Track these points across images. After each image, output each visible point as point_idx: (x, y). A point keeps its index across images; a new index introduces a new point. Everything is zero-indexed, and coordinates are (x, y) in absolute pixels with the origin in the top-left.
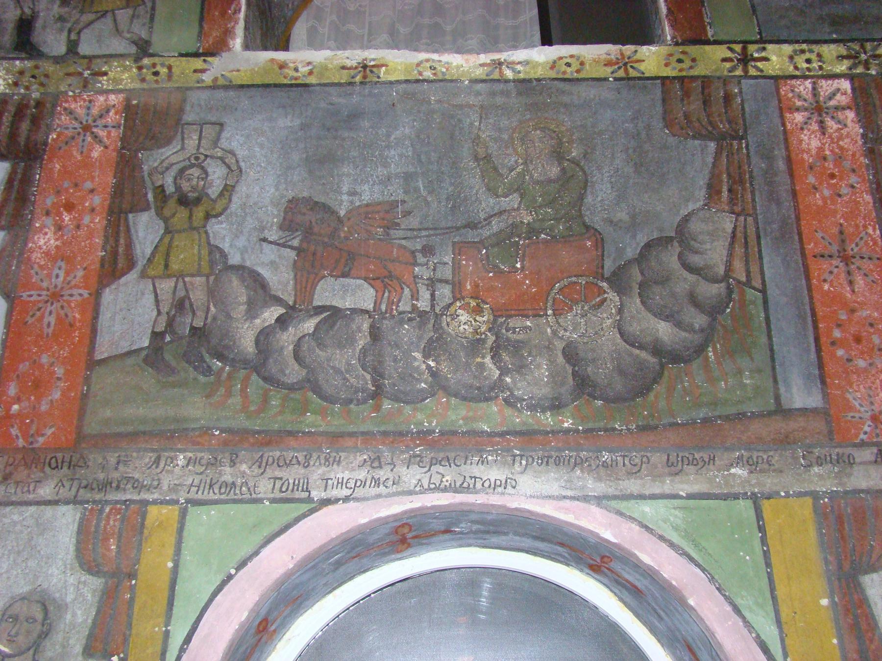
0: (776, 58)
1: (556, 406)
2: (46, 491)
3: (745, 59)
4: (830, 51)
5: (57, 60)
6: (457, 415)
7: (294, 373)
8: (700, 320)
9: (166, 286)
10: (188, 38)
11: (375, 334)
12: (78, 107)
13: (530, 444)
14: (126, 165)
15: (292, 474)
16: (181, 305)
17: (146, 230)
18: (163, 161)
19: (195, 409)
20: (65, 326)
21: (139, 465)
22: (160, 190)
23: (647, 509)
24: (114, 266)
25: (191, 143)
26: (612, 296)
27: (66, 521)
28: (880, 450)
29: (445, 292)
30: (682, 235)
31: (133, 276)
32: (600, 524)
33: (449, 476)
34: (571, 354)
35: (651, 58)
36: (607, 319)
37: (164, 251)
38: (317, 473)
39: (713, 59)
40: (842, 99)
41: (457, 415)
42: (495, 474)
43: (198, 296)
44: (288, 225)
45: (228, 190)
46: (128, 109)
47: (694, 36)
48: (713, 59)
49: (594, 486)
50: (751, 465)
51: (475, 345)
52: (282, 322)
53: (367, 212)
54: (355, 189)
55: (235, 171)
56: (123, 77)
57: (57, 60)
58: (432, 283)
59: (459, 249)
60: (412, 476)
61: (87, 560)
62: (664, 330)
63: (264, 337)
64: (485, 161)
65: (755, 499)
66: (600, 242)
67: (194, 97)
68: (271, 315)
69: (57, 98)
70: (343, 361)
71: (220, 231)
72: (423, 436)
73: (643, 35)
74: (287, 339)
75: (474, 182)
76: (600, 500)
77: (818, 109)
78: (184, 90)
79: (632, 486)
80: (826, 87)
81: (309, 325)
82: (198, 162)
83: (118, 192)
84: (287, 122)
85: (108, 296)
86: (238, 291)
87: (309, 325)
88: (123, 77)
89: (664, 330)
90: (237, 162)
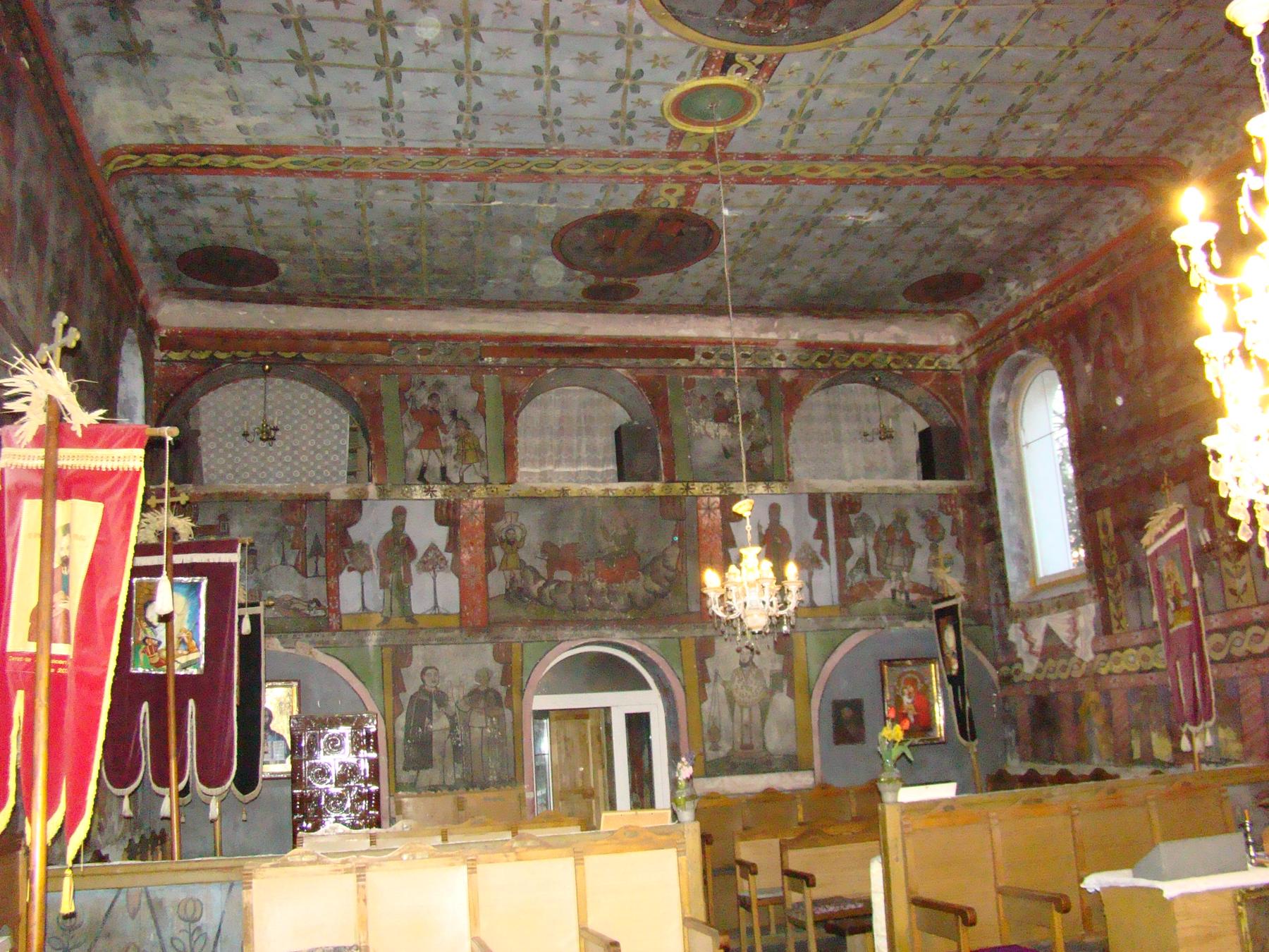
0: (697, 488)
1: (625, 612)
2: (482, 639)
3: (688, 488)
4: (715, 485)
5: (457, 485)
6: (596, 614)
7: (549, 602)
8: (667, 584)
9: (507, 573)
10: (502, 477)
11: (573, 589)
12: (468, 505)
13: (619, 623)
14: (488, 528)
15: (552, 633)
16: (513, 579)
17: (498, 552)
18: (500, 526)
19: (521, 613)
20: (478, 587)
21: (508, 631)
22: (501, 538)
23: (650, 642)
24: (490, 566)
25: (509, 519)
26: (642, 576)
27: (489, 648)
28: (1190, 3)
29: (592, 575)
30: (663, 555)
31: (496, 570)
32: (637, 646)
33: (595, 632)
34: (629, 595)
35: (657, 487)
36: (640, 584)
37: (505, 560)
38: (559, 632)
39: (677, 488)
40: (716, 505)
41: (596, 614)
42: (609, 632)
43: (518, 577)
44: (543, 551)
45: (523, 539)
46: (485, 506)
47: (671, 479)
48: (677, 488)
49: (635, 635)
50: (679, 629)
51: (602, 592)
52: (545, 585)
53: (567, 546)
54: (564, 538)
55: (525, 532)
56: (480, 492)
57: (457, 485)
58: (589, 572)
59: (597, 560)
60: (585, 633)
61: (497, 657)
62: (657, 587)
63: (540, 590)
64: (604, 528)
65: (679, 639)
66: (639, 558)
67: (507, 501)
68: (541, 583)
69: (460, 500)
70: (564, 599)
71: (522, 554)
72: (588, 621)
73: (655, 478)
74: (546, 591)
75: (601, 537)
76: (637, 639)
77: (709, 509)
78: (503, 499)
79: (646, 635)
80: (712, 500)
81: (553, 586)
82: (511, 528)
83: (487, 539)
84: (539, 513)
85: (490, 576)
86: (531, 577)
87: (553, 586)
88: (480, 492)
89: (657, 587)
90: (1131, 114)
